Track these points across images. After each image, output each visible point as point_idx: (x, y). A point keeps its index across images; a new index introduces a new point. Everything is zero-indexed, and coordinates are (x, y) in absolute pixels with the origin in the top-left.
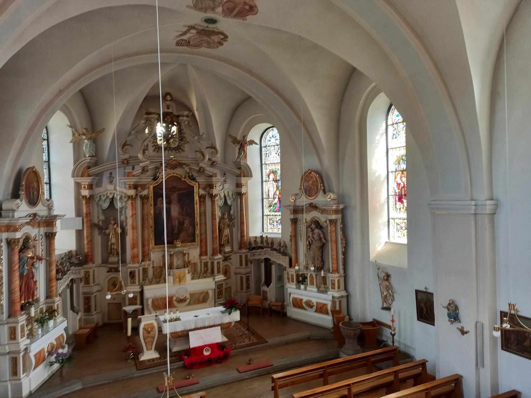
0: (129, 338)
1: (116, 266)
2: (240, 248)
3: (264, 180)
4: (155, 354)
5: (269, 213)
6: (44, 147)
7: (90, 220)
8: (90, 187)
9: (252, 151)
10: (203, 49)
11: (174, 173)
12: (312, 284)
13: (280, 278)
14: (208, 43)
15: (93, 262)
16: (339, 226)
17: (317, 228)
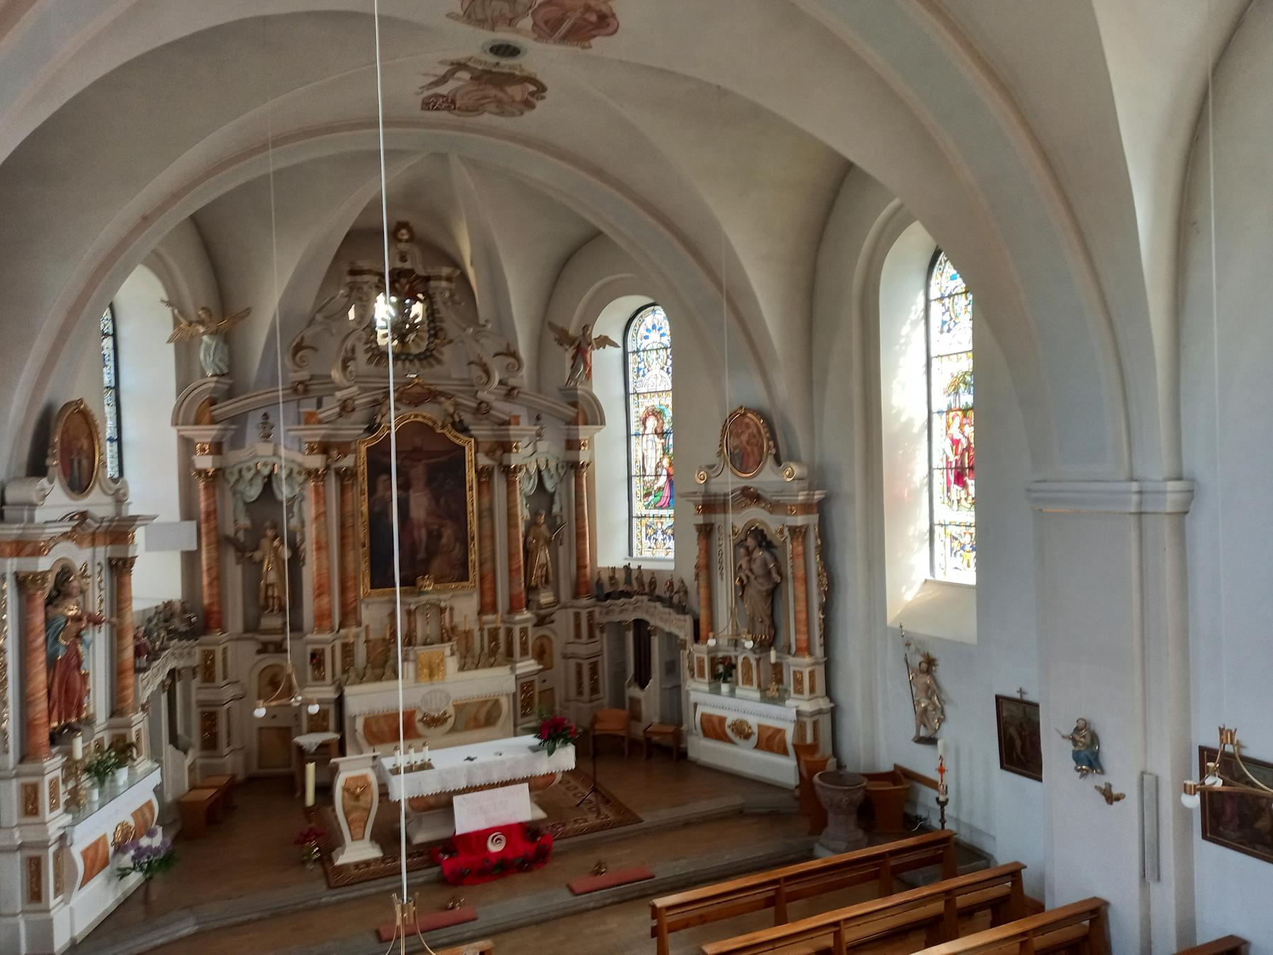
0: (308, 811)
1: (278, 638)
2: (576, 595)
3: (633, 432)
4: (371, 850)
5: (644, 512)
6: (105, 352)
7: (216, 527)
8: (216, 448)
9: (604, 362)
10: (487, 119)
11: (416, 416)
12: (748, 680)
13: (672, 668)
14: (499, 102)
15: (222, 628)
16: (813, 542)
17: (760, 546)
